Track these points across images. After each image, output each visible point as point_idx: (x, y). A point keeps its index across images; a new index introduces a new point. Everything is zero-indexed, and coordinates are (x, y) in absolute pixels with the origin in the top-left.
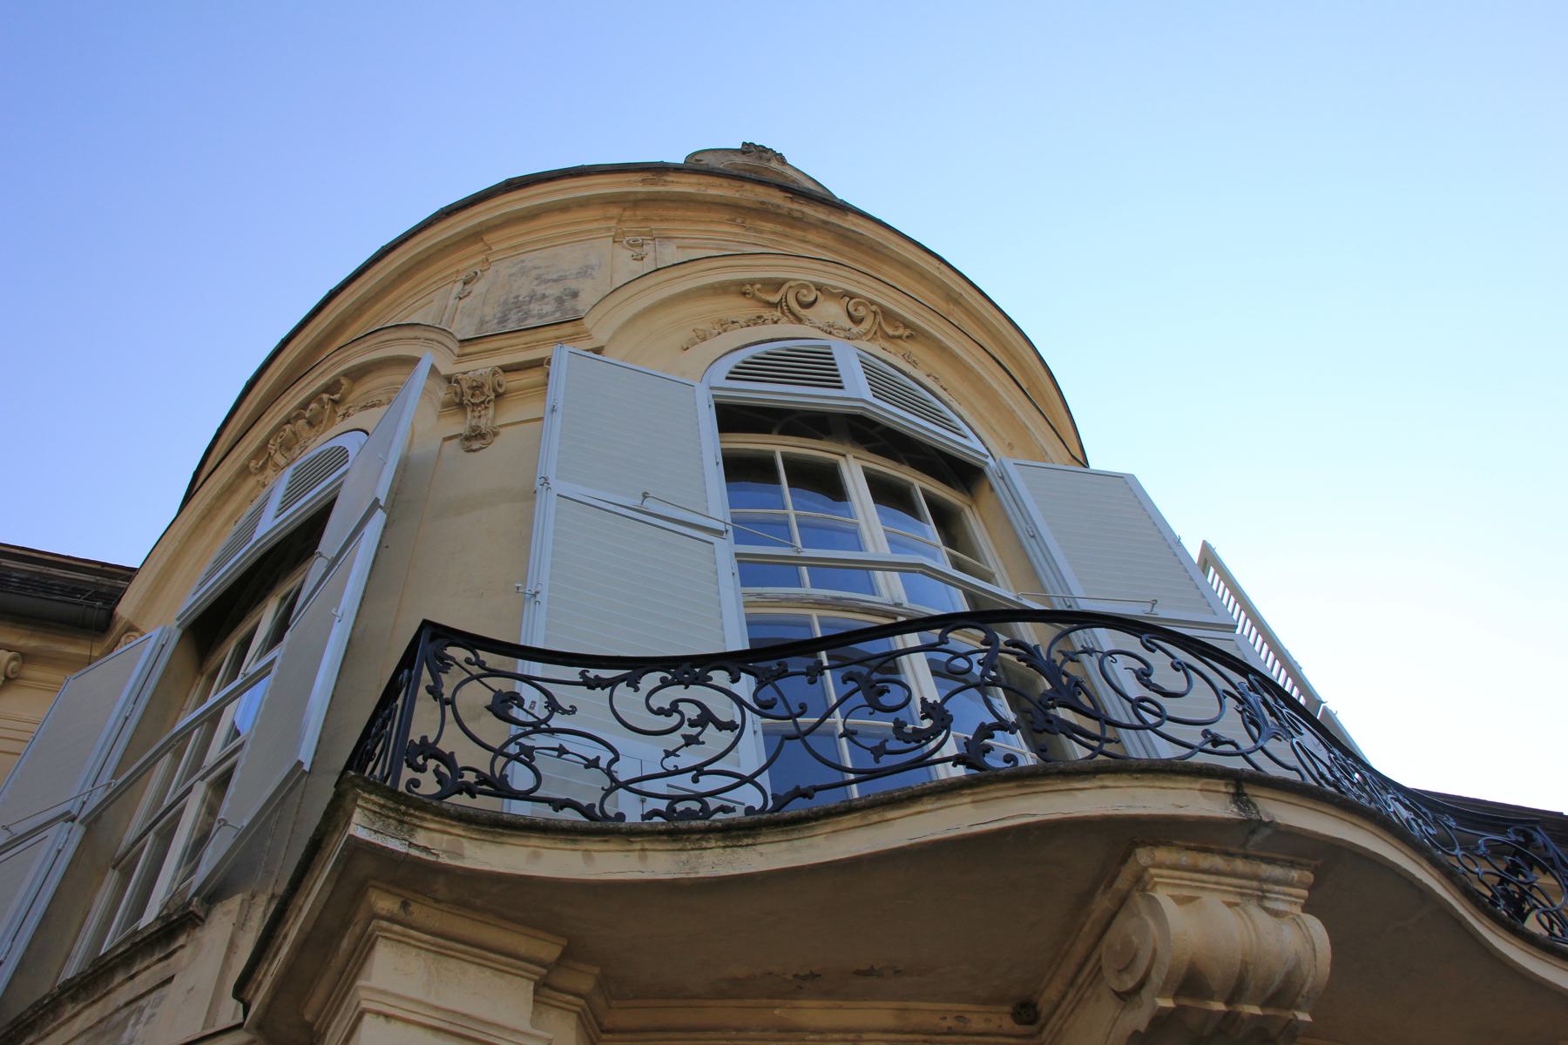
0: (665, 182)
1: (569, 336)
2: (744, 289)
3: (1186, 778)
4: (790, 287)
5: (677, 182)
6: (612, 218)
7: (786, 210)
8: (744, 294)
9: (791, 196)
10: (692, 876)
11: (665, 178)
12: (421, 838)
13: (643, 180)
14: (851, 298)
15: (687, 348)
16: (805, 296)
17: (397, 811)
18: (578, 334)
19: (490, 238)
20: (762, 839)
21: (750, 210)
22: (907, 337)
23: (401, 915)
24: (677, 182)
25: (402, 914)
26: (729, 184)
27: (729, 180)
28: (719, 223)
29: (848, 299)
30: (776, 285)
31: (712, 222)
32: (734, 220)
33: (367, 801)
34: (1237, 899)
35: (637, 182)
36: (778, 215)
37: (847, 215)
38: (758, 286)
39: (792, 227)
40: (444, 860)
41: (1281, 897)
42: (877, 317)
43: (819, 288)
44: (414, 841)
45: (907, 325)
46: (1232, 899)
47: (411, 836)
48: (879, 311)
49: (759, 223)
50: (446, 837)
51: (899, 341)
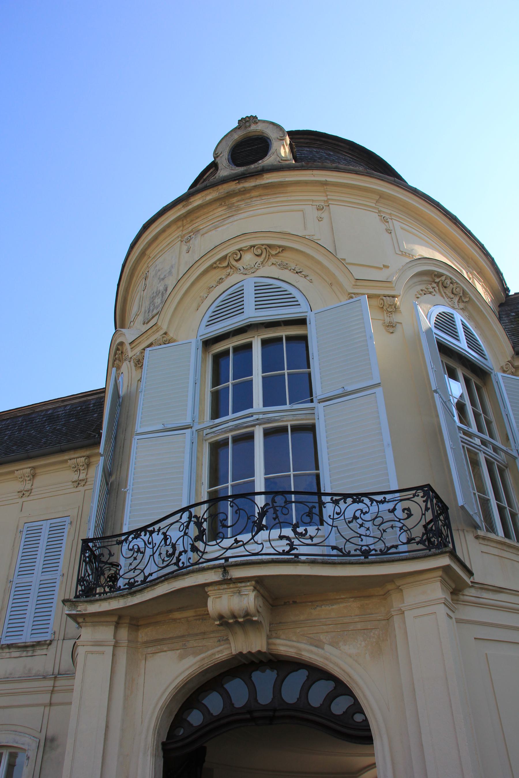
0: (190, 203)
1: (156, 330)
2: (214, 267)
3: (210, 570)
4: (229, 257)
5: (195, 200)
6: (180, 227)
7: (237, 190)
8: (215, 268)
9: (237, 181)
10: (126, 606)
11: (190, 201)
12: (79, 609)
13: (183, 206)
14: (254, 247)
15: (198, 309)
16: (236, 257)
17: (73, 604)
18: (158, 328)
19: (148, 252)
20: (137, 594)
21: (224, 198)
22: (282, 251)
23: (84, 621)
24: (195, 200)
25: (84, 621)
26: (213, 190)
27: (212, 188)
28: (216, 209)
29: (253, 248)
30: (224, 258)
31: (214, 210)
32: (221, 205)
33: (67, 604)
34: (233, 594)
35: (181, 208)
36: (236, 193)
37: (263, 175)
38: (218, 263)
39: (244, 194)
40: (84, 612)
41: (245, 591)
42: (267, 249)
43: (240, 250)
44: (78, 610)
45: (279, 247)
46: (231, 594)
47: (77, 609)
48: (267, 247)
49: (231, 200)
50: (84, 606)
51: (280, 254)
